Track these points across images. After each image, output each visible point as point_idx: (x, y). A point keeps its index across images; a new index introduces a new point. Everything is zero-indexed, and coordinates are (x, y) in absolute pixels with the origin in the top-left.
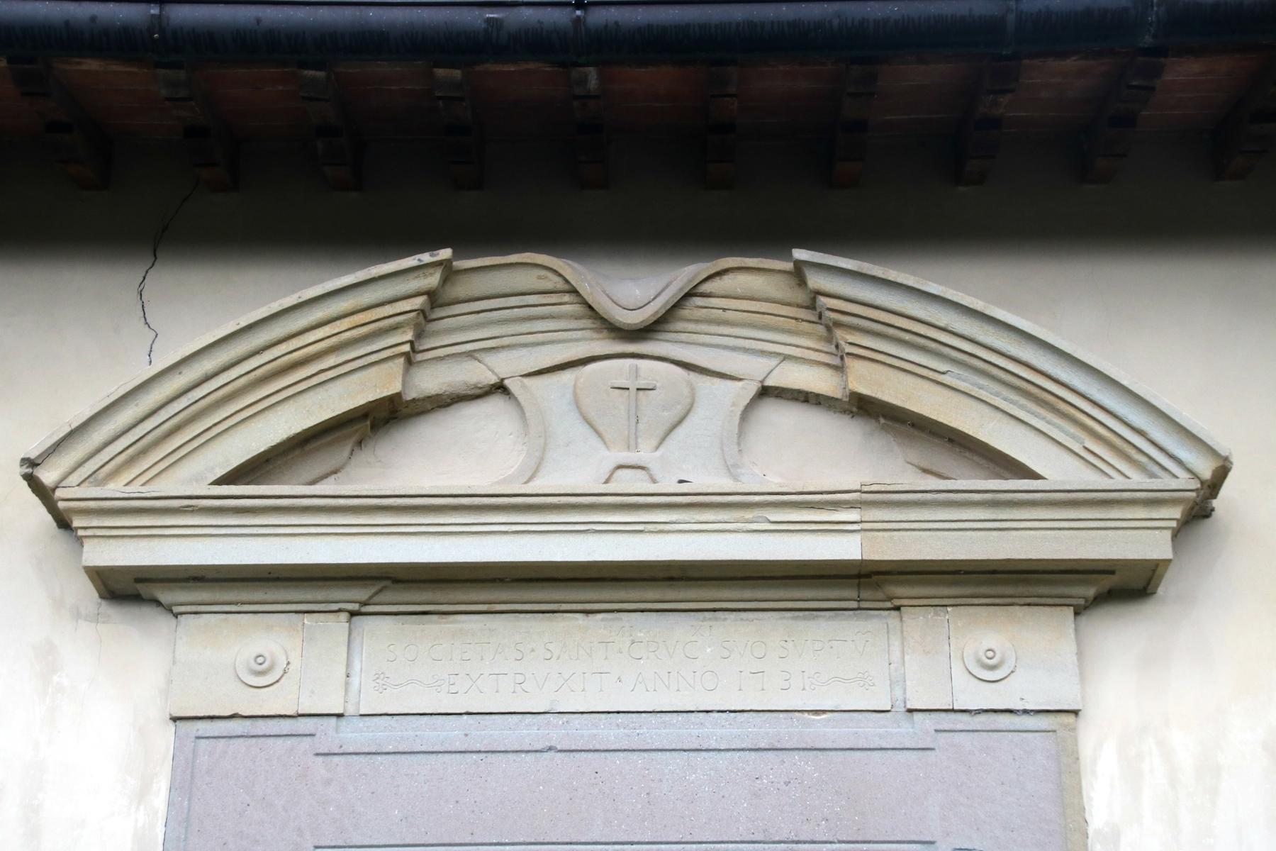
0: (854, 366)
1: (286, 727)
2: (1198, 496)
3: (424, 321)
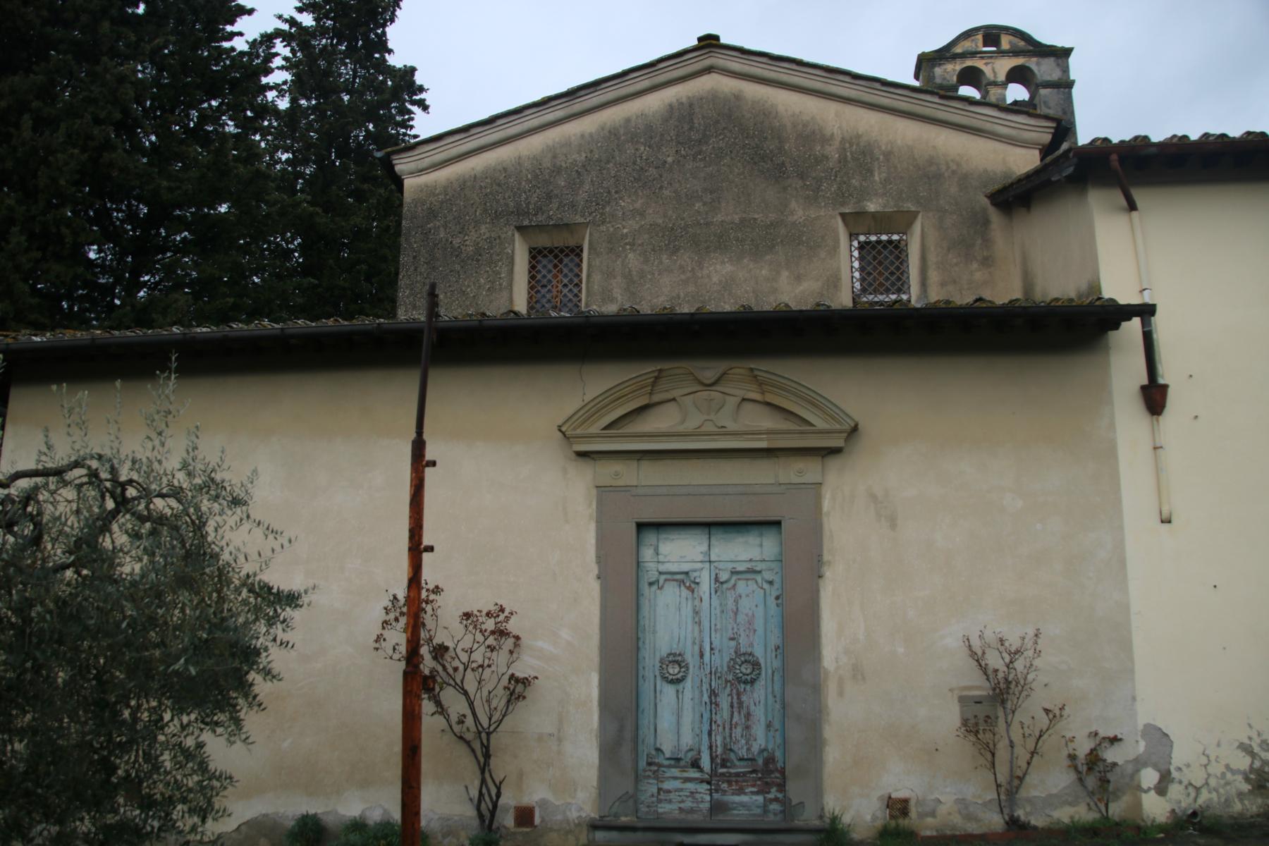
0: (767, 394)
2: (207, 541)
3: (654, 384)
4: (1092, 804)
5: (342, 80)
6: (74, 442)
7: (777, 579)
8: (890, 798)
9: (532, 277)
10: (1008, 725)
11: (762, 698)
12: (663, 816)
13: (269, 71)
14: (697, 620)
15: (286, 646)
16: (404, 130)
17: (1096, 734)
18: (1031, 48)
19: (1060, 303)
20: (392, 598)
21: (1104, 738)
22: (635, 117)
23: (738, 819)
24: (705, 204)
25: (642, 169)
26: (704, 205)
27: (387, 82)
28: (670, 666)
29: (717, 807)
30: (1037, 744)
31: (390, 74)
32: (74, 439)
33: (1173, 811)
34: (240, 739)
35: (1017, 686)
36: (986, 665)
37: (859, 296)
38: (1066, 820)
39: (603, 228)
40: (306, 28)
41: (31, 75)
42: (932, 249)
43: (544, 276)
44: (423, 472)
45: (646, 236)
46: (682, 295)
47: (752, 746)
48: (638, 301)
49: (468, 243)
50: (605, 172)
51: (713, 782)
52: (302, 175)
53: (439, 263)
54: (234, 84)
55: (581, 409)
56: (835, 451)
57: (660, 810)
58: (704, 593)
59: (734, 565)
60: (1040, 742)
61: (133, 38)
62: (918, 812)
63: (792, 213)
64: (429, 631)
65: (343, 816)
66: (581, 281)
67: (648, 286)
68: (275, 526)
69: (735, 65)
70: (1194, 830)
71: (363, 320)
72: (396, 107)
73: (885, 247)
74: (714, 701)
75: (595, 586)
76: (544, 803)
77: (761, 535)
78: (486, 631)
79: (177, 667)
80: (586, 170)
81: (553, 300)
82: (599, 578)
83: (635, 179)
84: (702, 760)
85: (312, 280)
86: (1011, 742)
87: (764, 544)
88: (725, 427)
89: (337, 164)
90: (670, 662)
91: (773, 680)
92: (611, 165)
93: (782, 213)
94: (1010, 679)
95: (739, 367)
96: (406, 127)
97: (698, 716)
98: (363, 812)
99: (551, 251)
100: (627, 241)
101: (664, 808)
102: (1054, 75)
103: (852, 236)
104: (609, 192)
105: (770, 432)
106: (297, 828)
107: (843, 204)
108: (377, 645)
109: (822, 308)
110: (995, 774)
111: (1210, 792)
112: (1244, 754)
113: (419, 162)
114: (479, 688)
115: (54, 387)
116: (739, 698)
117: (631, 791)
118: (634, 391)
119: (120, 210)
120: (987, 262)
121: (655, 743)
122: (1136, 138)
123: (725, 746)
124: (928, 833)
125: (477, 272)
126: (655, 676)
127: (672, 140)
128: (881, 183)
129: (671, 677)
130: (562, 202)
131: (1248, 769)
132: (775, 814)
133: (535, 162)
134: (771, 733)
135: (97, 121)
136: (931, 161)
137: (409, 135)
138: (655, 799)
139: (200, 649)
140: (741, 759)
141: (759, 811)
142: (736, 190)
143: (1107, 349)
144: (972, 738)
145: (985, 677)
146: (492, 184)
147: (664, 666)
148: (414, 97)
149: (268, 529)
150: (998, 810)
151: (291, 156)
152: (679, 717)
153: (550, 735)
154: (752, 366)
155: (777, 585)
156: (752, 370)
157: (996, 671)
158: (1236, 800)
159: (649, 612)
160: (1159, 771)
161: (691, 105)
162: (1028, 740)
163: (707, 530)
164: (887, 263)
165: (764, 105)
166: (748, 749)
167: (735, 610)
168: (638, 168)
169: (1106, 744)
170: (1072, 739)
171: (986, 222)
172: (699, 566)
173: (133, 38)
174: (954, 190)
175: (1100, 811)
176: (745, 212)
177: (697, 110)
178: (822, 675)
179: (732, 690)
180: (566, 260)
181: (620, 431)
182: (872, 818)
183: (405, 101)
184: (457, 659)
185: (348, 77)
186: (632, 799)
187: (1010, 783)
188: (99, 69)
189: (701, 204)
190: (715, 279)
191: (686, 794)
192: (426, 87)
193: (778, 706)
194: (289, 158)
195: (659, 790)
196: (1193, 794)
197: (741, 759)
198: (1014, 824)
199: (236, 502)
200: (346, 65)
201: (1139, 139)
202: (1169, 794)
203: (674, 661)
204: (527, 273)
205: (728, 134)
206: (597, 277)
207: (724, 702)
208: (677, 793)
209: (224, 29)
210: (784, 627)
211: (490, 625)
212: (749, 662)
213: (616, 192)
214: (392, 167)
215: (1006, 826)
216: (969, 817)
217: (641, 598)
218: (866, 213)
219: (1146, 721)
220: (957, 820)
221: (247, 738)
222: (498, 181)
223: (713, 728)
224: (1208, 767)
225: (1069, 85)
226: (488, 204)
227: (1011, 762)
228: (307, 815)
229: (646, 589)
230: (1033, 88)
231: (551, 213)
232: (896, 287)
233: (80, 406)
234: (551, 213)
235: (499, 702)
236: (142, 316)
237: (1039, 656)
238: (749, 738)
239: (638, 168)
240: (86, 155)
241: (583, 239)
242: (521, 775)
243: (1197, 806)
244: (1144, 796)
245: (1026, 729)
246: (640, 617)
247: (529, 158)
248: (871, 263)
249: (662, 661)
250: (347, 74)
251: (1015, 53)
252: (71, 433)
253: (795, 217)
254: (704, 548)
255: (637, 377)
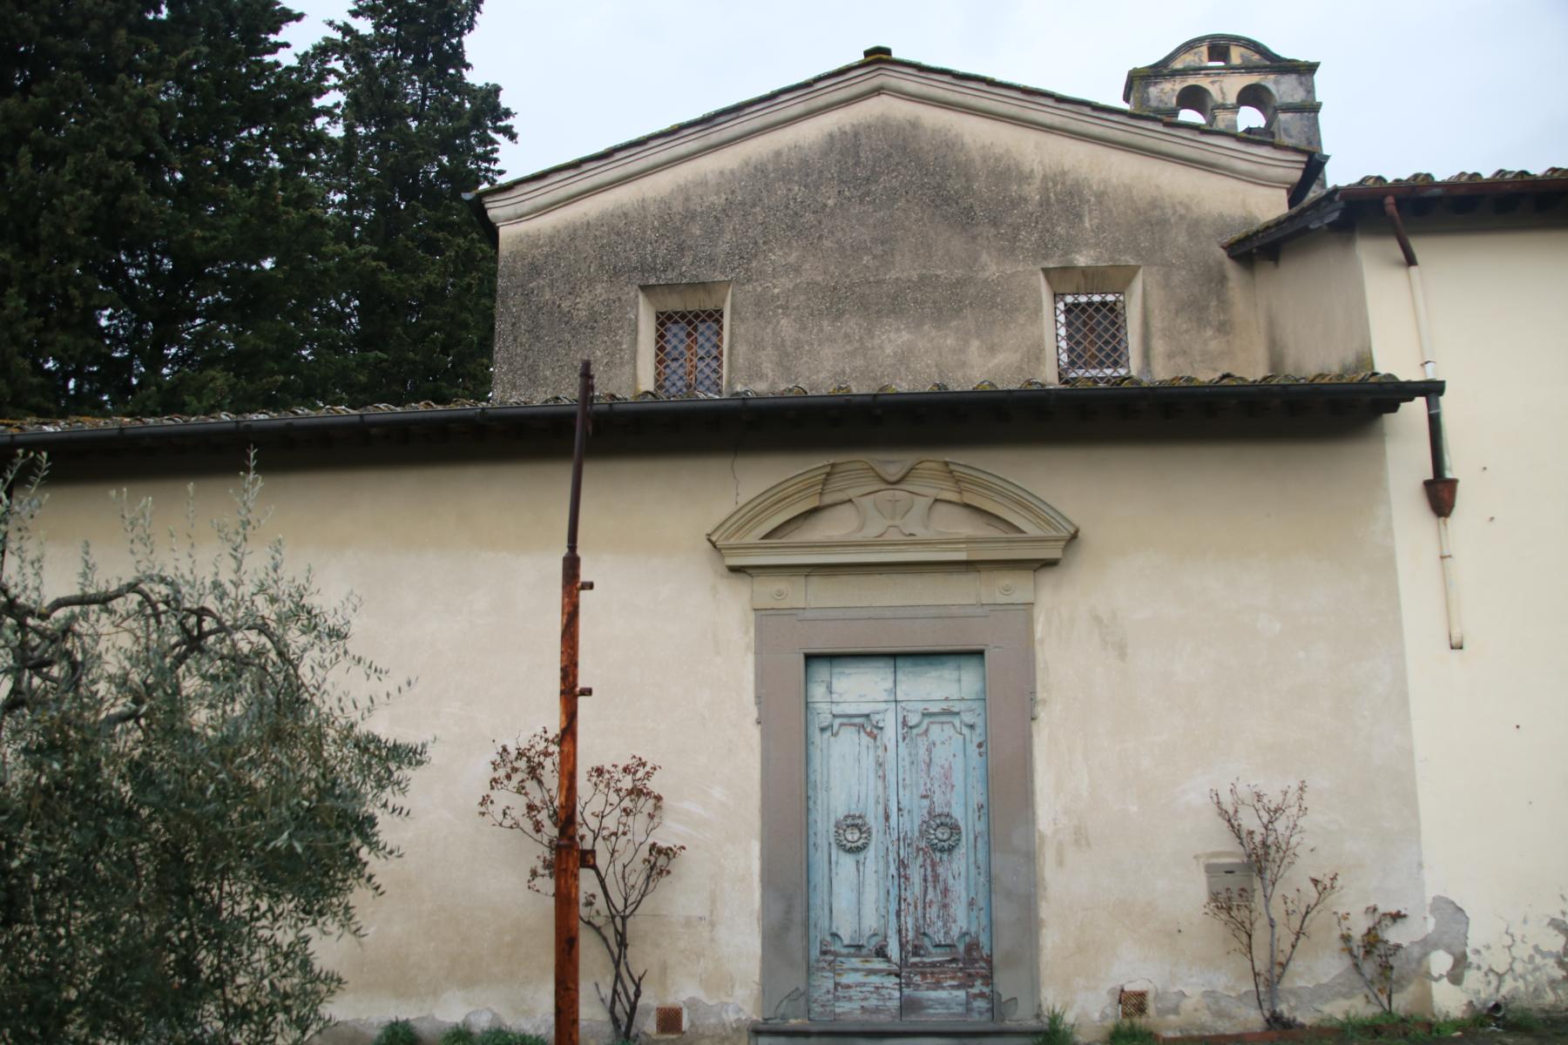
0: (965, 494)
1: (788, 612)
3: (825, 482)
4: (1371, 996)
5: (408, 102)
6: (138, 562)
7: (979, 722)
8: (1122, 991)
9: (661, 349)
10: (1267, 898)
11: (963, 870)
12: (841, 1017)
13: (321, 92)
14: (880, 773)
15: (400, 813)
16: (486, 165)
17: (1375, 910)
18: (1268, 63)
19: (1326, 380)
20: (500, 750)
21: (1384, 915)
22: (786, 149)
23: (934, 1019)
24: (875, 257)
25: (796, 214)
26: (873, 259)
27: (464, 104)
28: (849, 831)
29: (908, 1006)
30: (1303, 922)
31: (468, 95)
32: (138, 558)
33: (1471, 1003)
34: (350, 931)
35: (1278, 851)
36: (1239, 825)
37: (1066, 370)
38: (1340, 1016)
39: (749, 287)
40: (363, 38)
41: (31, 98)
42: (1157, 312)
43: (675, 347)
44: (577, 596)
45: (802, 298)
46: (848, 370)
47: (950, 929)
48: (793, 377)
49: (580, 306)
50: (750, 218)
51: (903, 974)
52: (358, 220)
53: (545, 332)
54: (281, 107)
55: (735, 513)
56: (1050, 564)
57: (838, 1010)
58: (889, 740)
59: (926, 705)
60: (1307, 919)
61: (156, 50)
62: (1157, 1008)
63: (983, 269)
64: (549, 791)
65: (443, 1022)
66: (721, 353)
67: (805, 359)
68: (378, 664)
69: (912, 85)
70: (1498, 1026)
71: (463, 404)
72: (476, 136)
73: (1097, 310)
74: (902, 874)
75: (755, 733)
76: (693, 1003)
77: (959, 668)
78: (621, 790)
79: (278, 845)
80: (727, 215)
81: (685, 377)
82: (759, 723)
83: (788, 227)
84: (889, 948)
85: (380, 354)
86: (1271, 920)
87: (962, 678)
88: (914, 535)
89: (402, 207)
90: (848, 826)
91: (975, 846)
92: (758, 209)
93: (971, 268)
94: (1269, 842)
95: (931, 460)
96: (489, 161)
97: (883, 893)
98: (467, 1016)
99: (683, 316)
100: (779, 303)
101: (842, 1007)
102: (1296, 97)
103: (1057, 296)
104: (756, 243)
105: (970, 541)
106: (384, 1038)
107: (1046, 257)
108: (483, 809)
109: (1034, 387)
110: (1252, 961)
111: (1515, 980)
112: (1556, 932)
113: (518, 205)
114: (612, 860)
115: (113, 493)
116: (933, 870)
117: (802, 988)
118: (801, 491)
119: (139, 266)
120: (1224, 328)
121: (831, 927)
122: (1416, 176)
123: (917, 929)
124: (1170, 1034)
125: (591, 343)
126: (830, 844)
127: (833, 178)
128: (1093, 231)
129: (849, 845)
130: (697, 255)
131: (1561, 951)
132: (981, 1013)
133: (662, 206)
134: (974, 913)
135: (113, 155)
136: (1154, 204)
137: (493, 171)
138: (831, 996)
139: (303, 821)
140: (937, 946)
141: (960, 1009)
142: (914, 240)
143: (1381, 436)
144: (1224, 916)
145: (1239, 841)
146: (609, 233)
147: (841, 831)
148: (499, 124)
149: (370, 667)
150: (1256, 1003)
151: (345, 197)
152: (859, 893)
153: (701, 918)
154: (947, 459)
155: (979, 730)
156: (946, 464)
157: (1251, 833)
158: (1548, 989)
159: (821, 764)
160: (1453, 954)
161: (856, 135)
162: (1292, 917)
163: (892, 662)
164: (1099, 329)
165: (946, 135)
166: (946, 933)
167: (928, 761)
168: (791, 213)
169: (1388, 921)
170: (1346, 917)
171: (1223, 279)
172: (882, 706)
173: (156, 50)
174: (1182, 239)
175: (1382, 1005)
176: (924, 267)
177: (864, 141)
178: (1037, 840)
179: (925, 860)
180: (702, 327)
181: (784, 540)
182: (1100, 1017)
183: (487, 127)
184: (584, 826)
185: (415, 98)
186: (803, 996)
187: (1270, 971)
188: (114, 89)
189: (870, 257)
190: (889, 351)
191: (869, 989)
192: (513, 111)
193: (982, 879)
194: (343, 200)
195: (837, 985)
196: (1495, 982)
197: (937, 946)
198: (1276, 1021)
199: (336, 634)
200: (413, 83)
201: (1420, 179)
202: (1465, 982)
203: (853, 825)
204: (653, 343)
205: (903, 171)
206: (742, 349)
207: (915, 874)
208: (858, 989)
209: (266, 39)
210: (988, 780)
211: (627, 783)
212: (946, 825)
213: (765, 243)
214: (485, 211)
215: (1265, 1023)
216: (1220, 1014)
217: (811, 748)
218: (1075, 268)
219: (1433, 895)
220: (1205, 1018)
221: (358, 930)
222: (616, 229)
223: (903, 907)
224: (1513, 949)
225: (1314, 108)
226: (605, 258)
227: (1271, 945)
228: (397, 1023)
229: (817, 736)
230: (1270, 112)
231: (684, 269)
232: (1111, 360)
233: (144, 516)
234: (684, 269)
235: (637, 878)
236: (171, 402)
237: (1305, 814)
238: (947, 920)
239: (791, 213)
240: (99, 197)
241: (724, 301)
242: (664, 969)
243: (1499, 997)
244: (1434, 985)
245: (1289, 904)
246: (810, 771)
247: (655, 201)
248: (1080, 330)
249: (837, 825)
250: (415, 94)
251: (1248, 68)
252: (135, 550)
253: (987, 274)
254: (889, 684)
255: (805, 473)
